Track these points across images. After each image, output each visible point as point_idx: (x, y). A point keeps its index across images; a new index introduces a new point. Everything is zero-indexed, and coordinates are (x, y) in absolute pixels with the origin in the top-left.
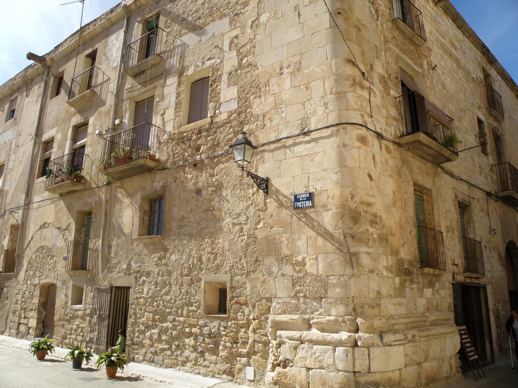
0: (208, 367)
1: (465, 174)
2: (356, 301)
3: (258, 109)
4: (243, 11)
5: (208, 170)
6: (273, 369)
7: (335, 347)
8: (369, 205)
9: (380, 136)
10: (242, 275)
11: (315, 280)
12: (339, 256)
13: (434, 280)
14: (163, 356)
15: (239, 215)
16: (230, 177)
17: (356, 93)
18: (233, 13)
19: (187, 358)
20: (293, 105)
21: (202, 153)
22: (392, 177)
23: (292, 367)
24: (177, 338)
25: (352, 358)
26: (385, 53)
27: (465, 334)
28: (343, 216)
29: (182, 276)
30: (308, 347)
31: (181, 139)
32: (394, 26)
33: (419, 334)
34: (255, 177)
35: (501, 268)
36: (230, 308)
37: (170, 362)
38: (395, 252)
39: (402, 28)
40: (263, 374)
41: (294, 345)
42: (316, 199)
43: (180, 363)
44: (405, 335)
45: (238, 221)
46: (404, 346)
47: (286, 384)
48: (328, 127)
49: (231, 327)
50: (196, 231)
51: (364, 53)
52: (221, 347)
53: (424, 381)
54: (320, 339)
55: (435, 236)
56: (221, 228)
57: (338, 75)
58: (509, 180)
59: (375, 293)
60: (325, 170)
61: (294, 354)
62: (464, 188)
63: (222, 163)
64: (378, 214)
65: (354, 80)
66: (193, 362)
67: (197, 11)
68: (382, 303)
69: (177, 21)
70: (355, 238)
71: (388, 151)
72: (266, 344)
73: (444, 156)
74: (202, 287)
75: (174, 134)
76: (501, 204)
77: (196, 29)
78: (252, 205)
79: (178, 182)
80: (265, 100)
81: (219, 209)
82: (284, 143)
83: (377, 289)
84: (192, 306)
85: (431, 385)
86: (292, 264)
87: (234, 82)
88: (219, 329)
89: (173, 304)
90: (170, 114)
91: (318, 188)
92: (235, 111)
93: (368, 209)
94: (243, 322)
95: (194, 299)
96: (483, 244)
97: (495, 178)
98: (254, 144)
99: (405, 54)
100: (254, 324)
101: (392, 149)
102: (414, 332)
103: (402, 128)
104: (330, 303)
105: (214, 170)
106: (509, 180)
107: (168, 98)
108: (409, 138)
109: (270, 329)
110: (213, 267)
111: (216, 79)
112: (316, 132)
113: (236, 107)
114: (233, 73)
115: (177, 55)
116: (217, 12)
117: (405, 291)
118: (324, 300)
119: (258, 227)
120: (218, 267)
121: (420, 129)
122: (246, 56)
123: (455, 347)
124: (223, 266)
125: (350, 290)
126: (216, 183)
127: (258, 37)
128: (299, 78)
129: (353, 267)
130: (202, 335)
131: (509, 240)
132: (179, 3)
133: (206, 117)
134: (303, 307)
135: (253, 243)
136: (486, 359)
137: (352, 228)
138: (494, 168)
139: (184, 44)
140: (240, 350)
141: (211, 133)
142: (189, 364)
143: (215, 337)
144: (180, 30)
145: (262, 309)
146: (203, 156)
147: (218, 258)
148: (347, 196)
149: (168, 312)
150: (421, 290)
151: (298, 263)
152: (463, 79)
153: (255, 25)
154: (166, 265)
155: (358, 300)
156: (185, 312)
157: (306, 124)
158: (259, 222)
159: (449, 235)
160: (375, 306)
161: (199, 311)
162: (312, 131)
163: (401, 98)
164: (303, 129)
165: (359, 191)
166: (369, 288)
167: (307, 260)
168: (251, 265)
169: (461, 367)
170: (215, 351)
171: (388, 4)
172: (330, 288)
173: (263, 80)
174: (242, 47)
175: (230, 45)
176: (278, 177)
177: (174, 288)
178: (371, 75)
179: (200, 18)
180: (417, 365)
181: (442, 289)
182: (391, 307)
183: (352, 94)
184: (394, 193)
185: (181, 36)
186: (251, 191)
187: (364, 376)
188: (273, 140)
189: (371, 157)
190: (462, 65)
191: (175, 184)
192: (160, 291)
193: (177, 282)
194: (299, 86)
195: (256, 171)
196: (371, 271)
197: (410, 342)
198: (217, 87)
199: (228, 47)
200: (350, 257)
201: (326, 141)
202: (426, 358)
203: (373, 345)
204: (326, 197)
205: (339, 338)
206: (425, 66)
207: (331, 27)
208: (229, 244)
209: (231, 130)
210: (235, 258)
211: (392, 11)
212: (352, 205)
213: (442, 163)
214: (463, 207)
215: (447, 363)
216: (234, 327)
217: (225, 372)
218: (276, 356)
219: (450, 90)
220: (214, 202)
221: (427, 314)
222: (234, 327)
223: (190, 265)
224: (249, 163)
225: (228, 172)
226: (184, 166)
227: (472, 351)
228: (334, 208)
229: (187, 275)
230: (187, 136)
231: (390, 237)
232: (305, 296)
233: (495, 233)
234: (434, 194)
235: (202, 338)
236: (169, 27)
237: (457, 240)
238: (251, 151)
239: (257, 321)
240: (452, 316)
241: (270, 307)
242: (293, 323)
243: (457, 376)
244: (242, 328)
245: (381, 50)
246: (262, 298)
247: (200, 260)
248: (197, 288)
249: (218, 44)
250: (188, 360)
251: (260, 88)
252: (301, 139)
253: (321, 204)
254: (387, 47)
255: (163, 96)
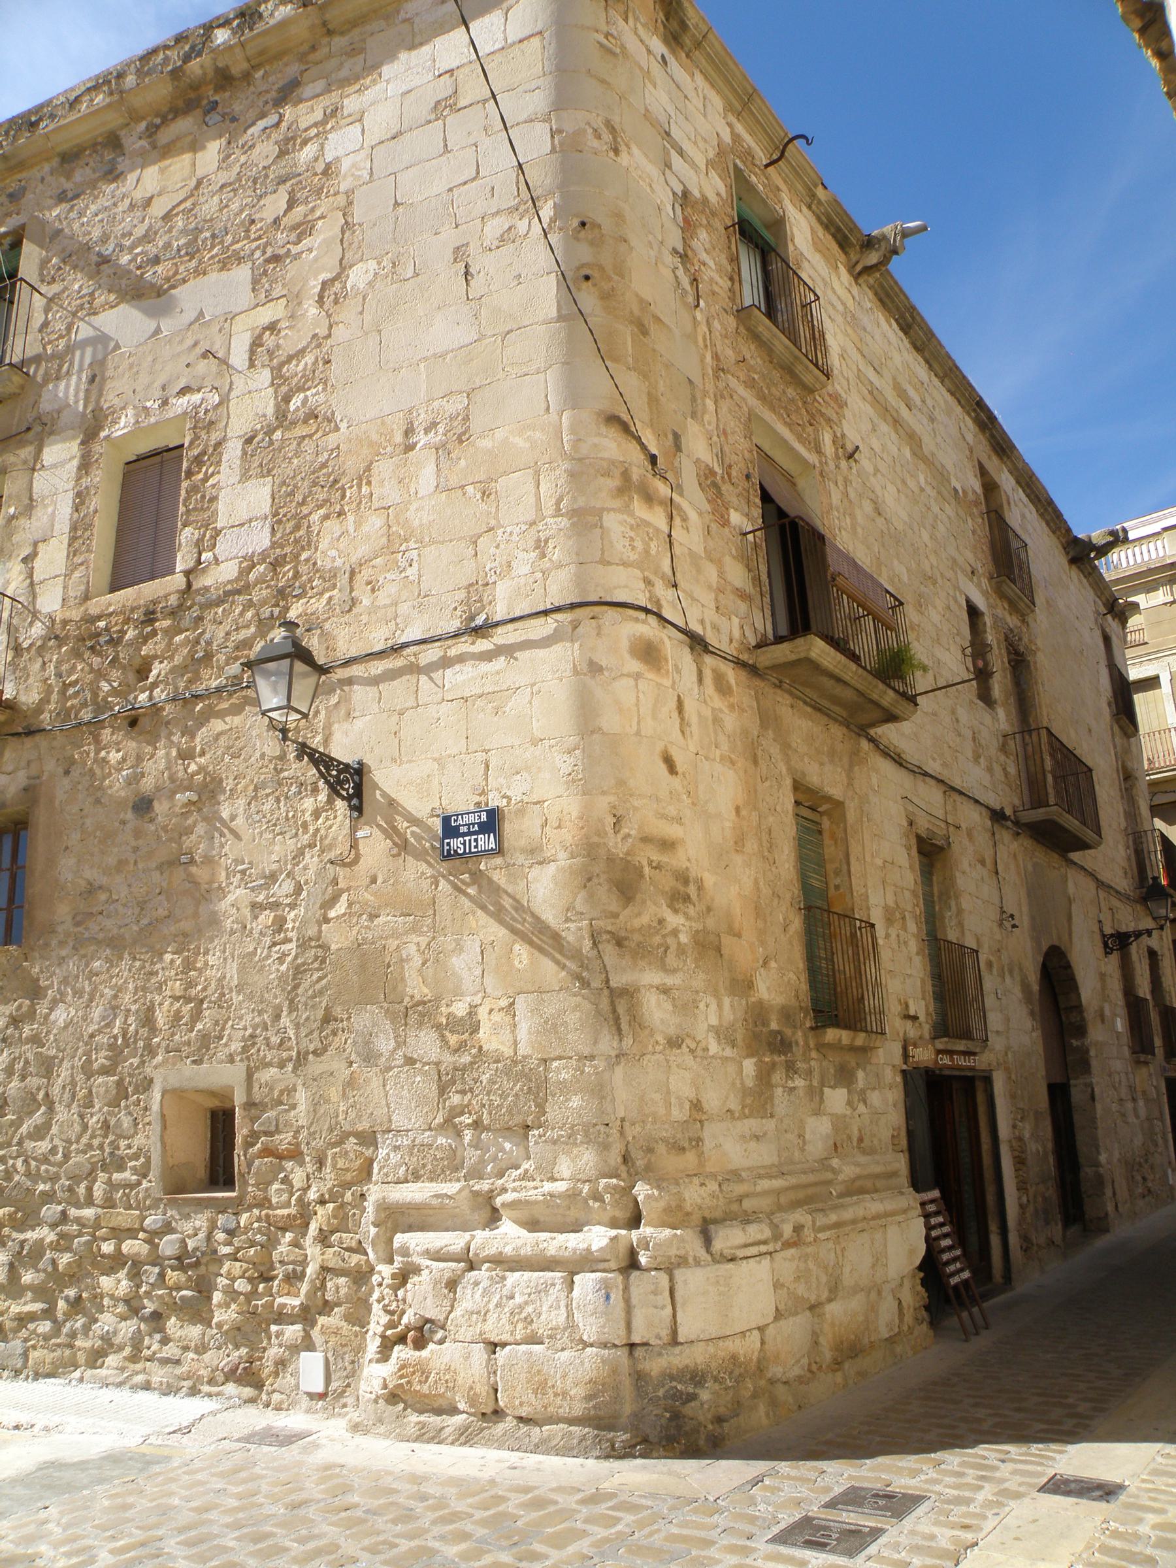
0: (178, 1362)
1: (934, 759)
2: (630, 1132)
3: (334, 553)
4: (295, 250)
5: (175, 739)
6: (385, 1353)
7: (573, 1274)
8: (667, 845)
9: (697, 643)
10: (282, 1065)
11: (507, 1072)
12: (579, 999)
13: (853, 1064)
14: (26, 1340)
15: (272, 878)
16: (245, 760)
17: (631, 514)
18: (264, 253)
19: (107, 1339)
20: (443, 542)
21: (155, 685)
22: (733, 763)
23: (441, 1342)
24: (73, 1276)
25: (622, 1304)
26: (716, 402)
27: (937, 1213)
28: (589, 880)
29: (89, 1074)
30: (492, 1278)
31: (89, 638)
32: (742, 329)
33: (814, 1222)
34: (322, 761)
35: (1028, 1023)
36: (244, 1169)
37: (49, 1357)
38: (742, 985)
39: (766, 335)
40: (353, 1373)
41: (447, 1275)
42: (508, 828)
43: (81, 1357)
44: (775, 1227)
45: (267, 897)
46: (772, 1260)
47: (425, 1396)
48: (545, 613)
49: (247, 1229)
50: (135, 928)
51: (657, 400)
52: (217, 1297)
53: (828, 1355)
54: (527, 1251)
55: (853, 935)
56: (214, 921)
57: (580, 460)
58: (1050, 778)
59: (687, 1106)
60: (535, 742)
61: (447, 1303)
62: (931, 797)
63: (221, 715)
64: (692, 874)
65: (626, 475)
66: (128, 1351)
67: (147, 238)
68: (706, 1134)
69: (81, 264)
70: (626, 943)
71: (722, 687)
72: (361, 1276)
73: (877, 704)
74: (155, 1107)
75: (65, 622)
76: (1028, 843)
77: (145, 293)
78: (311, 846)
79: (75, 773)
80: (358, 525)
81: (209, 860)
82: (412, 659)
83: (692, 1096)
84: (121, 1168)
85: (846, 1365)
86: (438, 1027)
87: (261, 465)
88: (209, 1237)
89: (60, 1165)
90: (53, 558)
91: (516, 794)
92: (264, 556)
93: (665, 859)
94: (286, 1212)
95: (129, 1147)
96: (983, 958)
97: (1012, 770)
98: (321, 660)
99: (773, 409)
100: (322, 1216)
101: (733, 682)
102: (800, 1216)
103: (762, 623)
104: (555, 1142)
105: (193, 736)
106: (1050, 778)
107: (46, 506)
108: (783, 652)
109: (373, 1230)
110: (188, 1043)
111: (204, 453)
112: (510, 626)
113: (267, 543)
114: (260, 437)
115: (81, 370)
116: (213, 247)
117: (772, 1098)
118: (536, 1132)
119: (332, 914)
120: (206, 1041)
121: (814, 628)
122: (301, 389)
123: (912, 1252)
124: (220, 1038)
125: (613, 1100)
126: (199, 778)
127: (339, 333)
128: (463, 462)
129: (619, 1030)
130: (156, 1259)
131: (1050, 943)
132: (87, 207)
133: (171, 571)
134: (471, 1156)
135: (316, 965)
136: (989, 1277)
137: (615, 916)
138: (1011, 743)
139: (101, 339)
140: (279, 1300)
141: (186, 623)
142: (112, 1360)
143: (197, 1264)
144: (92, 294)
145: (347, 1170)
146: (160, 694)
147: (207, 1013)
148: (600, 820)
149: (43, 1193)
150: (815, 1094)
151: (454, 1024)
152: (928, 489)
153: (331, 293)
154: (36, 1040)
155: (638, 1129)
156: (98, 1190)
157: (480, 600)
158: (334, 899)
159: (893, 932)
160: (686, 1145)
161: (145, 1184)
162: (497, 625)
163: (758, 533)
164: (472, 618)
165: (636, 804)
166: (668, 1092)
167: (482, 1013)
168: (311, 1032)
169: (927, 1308)
170: (197, 1310)
171: (725, 262)
172: (553, 1096)
173: (352, 465)
174: (290, 358)
175: (252, 352)
176: (394, 760)
177: (62, 1114)
178: (676, 464)
179: (156, 260)
180: (808, 1313)
181: (874, 1089)
182: (733, 1146)
183: (620, 517)
184: (738, 810)
185: (95, 314)
186: (308, 804)
187: (660, 1354)
188: (378, 647)
189: (673, 704)
190: (926, 451)
191: (66, 782)
192: (17, 1124)
193: (74, 1096)
194: (462, 487)
195: (326, 742)
196: (674, 1043)
197: (787, 1245)
198: (206, 479)
199: (246, 356)
200: (612, 1003)
201: (540, 653)
202: (834, 1290)
203: (682, 1261)
204: (539, 822)
205: (583, 1246)
206: (828, 448)
207: (561, 318)
208: (242, 970)
209: (249, 615)
210: (260, 1013)
211: (737, 284)
212: (617, 845)
213: (873, 725)
214: (931, 853)
215: (890, 1298)
216: (259, 1229)
217: (231, 1375)
218: (392, 1313)
219: (892, 518)
220: (193, 837)
221: (835, 1162)
222: (259, 1231)
223: (115, 1037)
224: (305, 716)
225: (239, 744)
226: (95, 726)
227: (954, 1260)
228: (562, 855)
229: (105, 1071)
230: (107, 629)
231: (727, 941)
232: (477, 1125)
233: (1014, 926)
234: (851, 816)
235: (157, 1270)
236: (54, 280)
237: (913, 945)
238: (311, 681)
239: (331, 1206)
240: (901, 1164)
241: (370, 1162)
242: (442, 1207)
243: (916, 1333)
244: (284, 1230)
245: (705, 394)
246: (347, 1135)
247: (148, 1020)
248: (137, 1111)
249: (212, 344)
250: (112, 1345)
251: (343, 489)
252: (464, 646)
253: (523, 843)
254: (721, 385)
255: (31, 499)
